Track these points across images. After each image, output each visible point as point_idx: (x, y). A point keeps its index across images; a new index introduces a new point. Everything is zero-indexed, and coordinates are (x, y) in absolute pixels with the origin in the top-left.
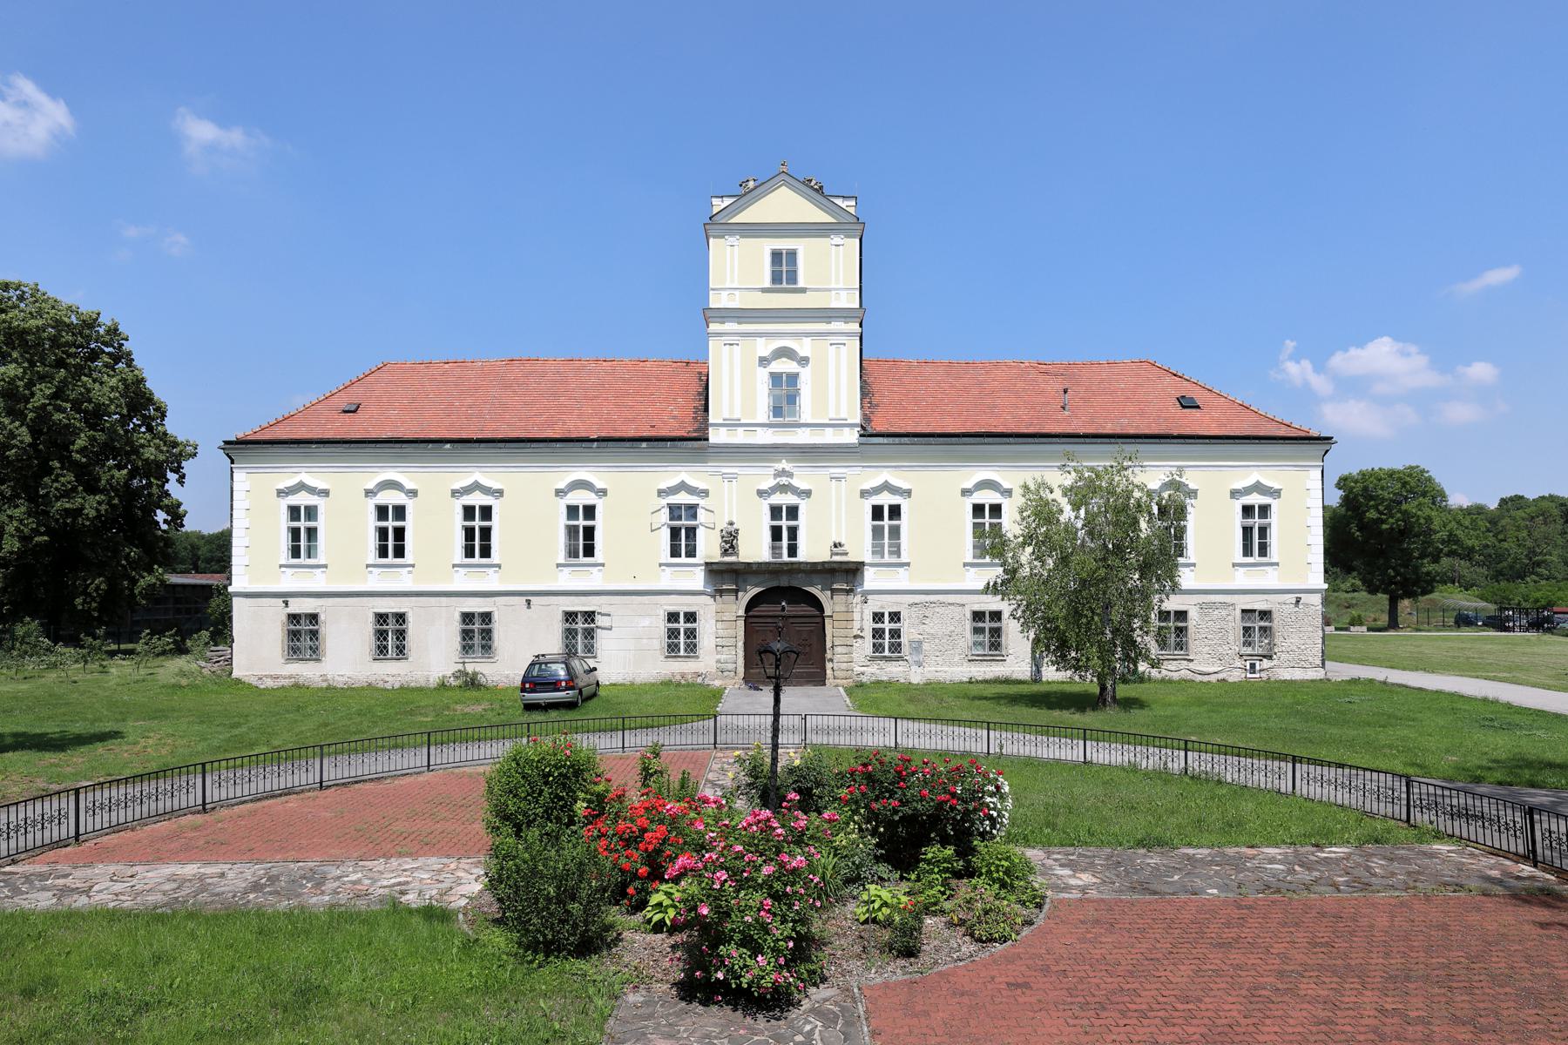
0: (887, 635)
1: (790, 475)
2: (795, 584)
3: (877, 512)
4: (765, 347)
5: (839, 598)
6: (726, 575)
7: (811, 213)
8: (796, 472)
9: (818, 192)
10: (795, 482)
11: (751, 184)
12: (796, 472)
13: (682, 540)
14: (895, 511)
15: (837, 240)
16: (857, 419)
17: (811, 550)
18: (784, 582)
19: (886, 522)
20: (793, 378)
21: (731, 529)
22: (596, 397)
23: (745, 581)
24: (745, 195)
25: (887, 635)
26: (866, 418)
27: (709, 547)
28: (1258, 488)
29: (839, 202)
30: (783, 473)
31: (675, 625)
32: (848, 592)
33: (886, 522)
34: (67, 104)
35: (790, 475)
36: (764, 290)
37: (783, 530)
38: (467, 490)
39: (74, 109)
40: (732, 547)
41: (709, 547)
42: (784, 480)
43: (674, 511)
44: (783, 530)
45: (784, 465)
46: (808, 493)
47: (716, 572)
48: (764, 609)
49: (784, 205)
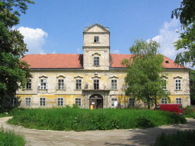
0: (43, 104)
1: (97, 75)
2: (98, 94)
3: (113, 81)
4: (93, 52)
5: (106, 96)
6: (85, 92)
7: (100, 30)
8: (98, 74)
9: (102, 27)
10: (98, 76)
11: (91, 26)
12: (98, 74)
13: (78, 85)
14: (116, 81)
15: (105, 35)
16: (109, 65)
17: (101, 87)
18: (96, 93)
19: (114, 83)
20: (98, 58)
21: (87, 84)
22: (63, 61)
23: (89, 93)
24: (90, 28)
25: (43, 104)
26: (111, 65)
27: (83, 87)
28: (178, 77)
29: (105, 28)
30: (95, 74)
31: (59, 101)
32: (107, 95)
33: (114, 83)
34: (38, 28)
35: (97, 75)
36: (93, 43)
37: (96, 85)
38: (77, 77)
39: (44, 30)
40: (87, 87)
41: (83, 87)
42: (96, 76)
43: (77, 81)
44: (96, 85)
45: (96, 73)
46: (100, 78)
47: (84, 91)
48: (91, 98)
49: (96, 29)
